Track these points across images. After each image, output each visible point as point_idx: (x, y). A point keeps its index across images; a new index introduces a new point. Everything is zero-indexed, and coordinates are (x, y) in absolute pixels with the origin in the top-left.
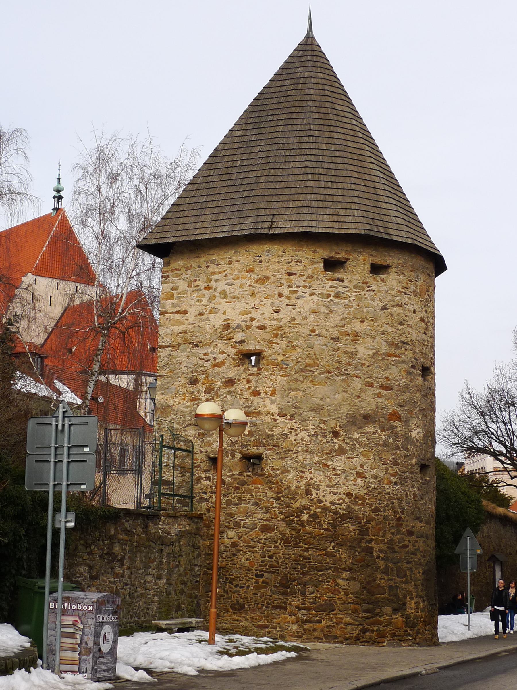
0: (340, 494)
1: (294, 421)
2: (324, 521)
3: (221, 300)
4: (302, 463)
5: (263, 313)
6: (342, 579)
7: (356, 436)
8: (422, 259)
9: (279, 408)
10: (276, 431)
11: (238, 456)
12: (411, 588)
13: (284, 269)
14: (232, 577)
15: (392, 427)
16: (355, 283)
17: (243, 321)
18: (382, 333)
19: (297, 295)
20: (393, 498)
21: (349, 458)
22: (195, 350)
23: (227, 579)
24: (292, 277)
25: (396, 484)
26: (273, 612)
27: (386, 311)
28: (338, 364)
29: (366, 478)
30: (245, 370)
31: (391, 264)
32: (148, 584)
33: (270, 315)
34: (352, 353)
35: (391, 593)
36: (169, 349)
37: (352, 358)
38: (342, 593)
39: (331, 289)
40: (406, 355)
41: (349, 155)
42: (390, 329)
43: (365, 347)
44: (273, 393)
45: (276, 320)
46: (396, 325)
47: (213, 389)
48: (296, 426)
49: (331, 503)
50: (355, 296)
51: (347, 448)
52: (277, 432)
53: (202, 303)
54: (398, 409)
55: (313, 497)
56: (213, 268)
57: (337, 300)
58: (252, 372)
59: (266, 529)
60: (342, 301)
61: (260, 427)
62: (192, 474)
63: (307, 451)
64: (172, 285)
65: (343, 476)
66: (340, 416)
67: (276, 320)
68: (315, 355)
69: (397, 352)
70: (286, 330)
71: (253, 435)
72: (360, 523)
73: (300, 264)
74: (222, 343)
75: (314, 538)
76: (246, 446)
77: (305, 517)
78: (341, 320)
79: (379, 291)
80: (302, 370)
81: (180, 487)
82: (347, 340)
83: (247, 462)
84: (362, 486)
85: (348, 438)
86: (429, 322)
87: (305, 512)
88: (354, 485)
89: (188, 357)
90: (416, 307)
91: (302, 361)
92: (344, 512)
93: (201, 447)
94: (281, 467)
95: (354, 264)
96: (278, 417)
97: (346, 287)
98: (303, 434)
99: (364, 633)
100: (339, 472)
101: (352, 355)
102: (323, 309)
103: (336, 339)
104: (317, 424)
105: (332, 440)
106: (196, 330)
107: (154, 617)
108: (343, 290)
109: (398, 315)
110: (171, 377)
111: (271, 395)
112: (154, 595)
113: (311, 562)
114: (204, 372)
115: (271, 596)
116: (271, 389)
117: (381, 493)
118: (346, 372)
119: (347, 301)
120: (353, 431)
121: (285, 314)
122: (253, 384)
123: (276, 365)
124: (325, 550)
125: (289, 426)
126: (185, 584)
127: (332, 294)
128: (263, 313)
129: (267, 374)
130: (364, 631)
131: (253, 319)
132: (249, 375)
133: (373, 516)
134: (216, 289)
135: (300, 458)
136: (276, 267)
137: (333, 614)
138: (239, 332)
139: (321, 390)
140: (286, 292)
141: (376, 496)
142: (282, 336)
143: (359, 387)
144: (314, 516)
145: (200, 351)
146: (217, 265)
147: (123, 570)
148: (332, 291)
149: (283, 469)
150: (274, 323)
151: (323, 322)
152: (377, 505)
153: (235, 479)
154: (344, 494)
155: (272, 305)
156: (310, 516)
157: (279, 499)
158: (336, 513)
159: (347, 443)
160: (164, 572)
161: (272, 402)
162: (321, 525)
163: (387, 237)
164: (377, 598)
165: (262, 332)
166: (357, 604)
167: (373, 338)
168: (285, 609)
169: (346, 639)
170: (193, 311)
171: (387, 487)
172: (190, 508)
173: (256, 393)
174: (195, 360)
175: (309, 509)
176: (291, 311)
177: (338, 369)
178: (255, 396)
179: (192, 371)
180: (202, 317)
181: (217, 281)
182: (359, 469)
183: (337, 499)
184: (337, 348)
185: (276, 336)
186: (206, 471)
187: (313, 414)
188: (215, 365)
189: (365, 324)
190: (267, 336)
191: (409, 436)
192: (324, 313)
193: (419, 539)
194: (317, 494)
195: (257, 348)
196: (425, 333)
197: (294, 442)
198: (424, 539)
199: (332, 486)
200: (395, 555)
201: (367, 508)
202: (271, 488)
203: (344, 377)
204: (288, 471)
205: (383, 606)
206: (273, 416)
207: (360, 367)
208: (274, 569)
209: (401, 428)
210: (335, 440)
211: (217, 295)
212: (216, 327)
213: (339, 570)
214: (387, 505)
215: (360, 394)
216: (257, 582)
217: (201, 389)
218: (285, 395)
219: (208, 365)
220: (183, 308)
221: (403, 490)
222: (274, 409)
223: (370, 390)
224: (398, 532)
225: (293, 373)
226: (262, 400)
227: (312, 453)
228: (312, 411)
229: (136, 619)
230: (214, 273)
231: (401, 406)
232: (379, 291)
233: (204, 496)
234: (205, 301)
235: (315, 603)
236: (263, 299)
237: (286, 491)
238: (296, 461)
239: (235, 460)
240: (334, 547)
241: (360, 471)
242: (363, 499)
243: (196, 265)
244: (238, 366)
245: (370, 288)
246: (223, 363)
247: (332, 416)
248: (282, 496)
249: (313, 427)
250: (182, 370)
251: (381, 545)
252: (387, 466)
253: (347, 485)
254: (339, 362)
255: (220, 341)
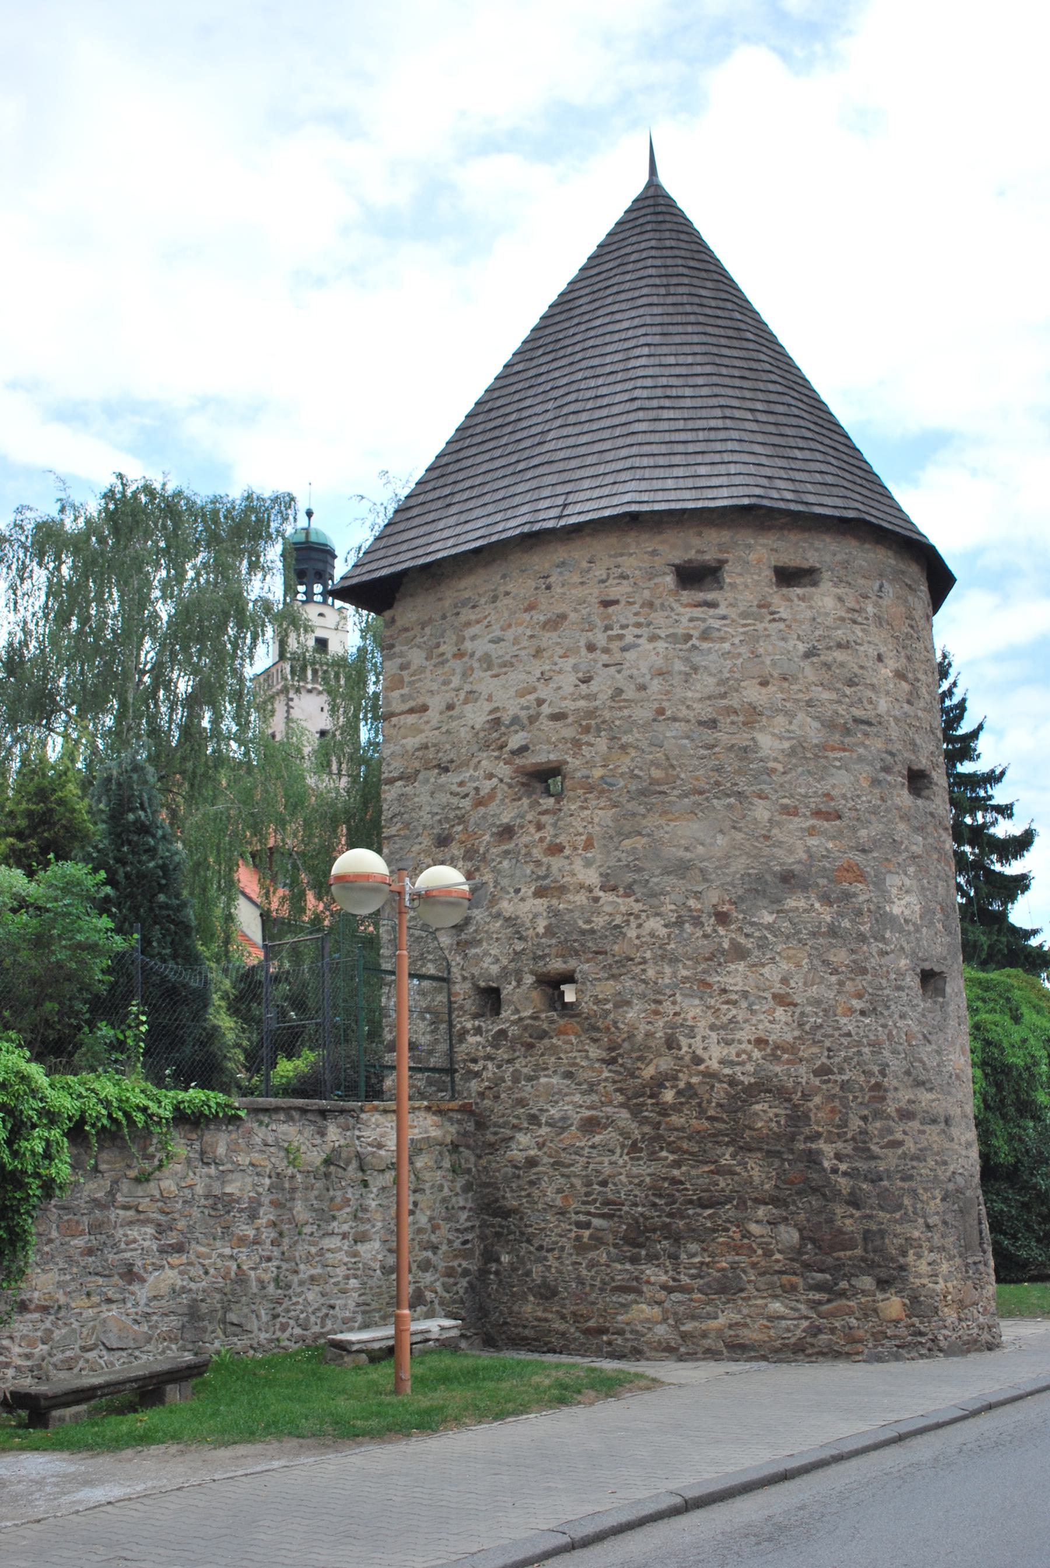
0: (740, 1042)
1: (632, 898)
2: (709, 1102)
3: (482, 674)
4: (656, 983)
5: (560, 688)
6: (757, 1222)
7: (768, 918)
8: (890, 553)
9: (601, 875)
10: (599, 922)
11: (529, 980)
12: (916, 1234)
13: (594, 593)
14: (530, 1230)
15: (847, 896)
16: (742, 607)
17: (522, 708)
18: (809, 703)
19: (623, 644)
20: (859, 1044)
21: (754, 966)
22: (443, 779)
23: (522, 1234)
24: (610, 609)
25: (863, 1013)
26: (614, 1299)
27: (815, 659)
28: (716, 774)
29: (796, 1005)
30: (531, 806)
31: (818, 565)
32: (329, 1255)
33: (572, 689)
34: (745, 749)
35: (870, 1247)
36: (400, 783)
37: (747, 758)
38: (760, 1252)
39: (692, 625)
40: (866, 747)
41: (724, 371)
42: (826, 695)
43: (773, 735)
44: (588, 845)
45: (587, 697)
46: (839, 685)
47: (477, 851)
48: (637, 907)
49: (722, 1062)
50: (744, 633)
51: (750, 946)
52: (601, 924)
53: (452, 686)
54: (859, 858)
55: (682, 1052)
56: (467, 614)
57: (705, 645)
58: (545, 807)
59: (591, 1125)
60: (717, 646)
61: (566, 917)
62: (451, 1025)
63: (663, 957)
64: (399, 661)
65: (744, 1004)
66: (729, 880)
67: (587, 697)
68: (668, 759)
69: (847, 740)
70: (607, 714)
71: (554, 935)
72: (789, 1100)
73: (625, 582)
74: (489, 757)
75: (690, 1138)
76: (542, 957)
77: (669, 1096)
78: (718, 685)
79: (795, 620)
80: (643, 793)
81: (431, 1052)
82: (733, 723)
83: (550, 991)
84: (787, 1024)
85: (753, 924)
86: (918, 680)
87: (667, 1084)
88: (770, 1022)
89: (433, 793)
90: (883, 649)
91: (641, 774)
92: (753, 1080)
93: (462, 969)
94: (612, 995)
95: (739, 570)
96: (601, 894)
97: (724, 618)
98: (654, 924)
99: (815, 1336)
100: (734, 997)
101: (745, 752)
102: (679, 666)
103: (712, 724)
104: (680, 899)
105: (715, 931)
106: (444, 738)
107: (347, 1324)
108: (717, 623)
109: (842, 665)
110: (406, 838)
111: (585, 849)
112: (347, 1278)
113: (687, 1189)
114: (461, 819)
115: (608, 1266)
116: (584, 837)
117: (832, 1036)
118: (735, 788)
119: (727, 646)
120: (759, 908)
121: (602, 685)
122: (548, 833)
123: (590, 789)
124: (716, 1161)
125: (623, 909)
126: (435, 1248)
127: (696, 633)
128: (560, 688)
129: (573, 807)
130: (815, 1331)
131: (540, 702)
132: (540, 813)
133: (817, 1083)
134: (472, 655)
135: (651, 973)
136: (578, 592)
137: (743, 1299)
138: (516, 732)
139: (688, 829)
140: (600, 639)
141: (820, 1042)
142: (599, 730)
143: (766, 818)
144: (688, 1092)
145: (451, 779)
146: (474, 607)
147: (258, 1229)
148: (694, 628)
149: (618, 998)
150: (582, 703)
151: (679, 693)
152: (825, 1060)
153: (526, 1028)
154: (749, 1042)
155: (575, 668)
156: (679, 1093)
157: (613, 1061)
158: (732, 1082)
159: (747, 935)
160: (373, 1226)
161: (588, 863)
162: (702, 1111)
163: (801, 508)
164: (838, 1259)
165: (559, 724)
166: (795, 1274)
167: (791, 715)
168: (639, 1292)
169: (777, 1351)
170: (436, 704)
171: (844, 1020)
172: (450, 1093)
173: (556, 849)
174: (443, 798)
175: (676, 1078)
176: (613, 678)
177: (718, 784)
178: (553, 854)
179: (440, 821)
180: (451, 713)
181: (473, 638)
182: (778, 988)
183: (734, 1052)
184: (713, 742)
185: (587, 730)
186: (475, 1016)
187: (672, 880)
188: (480, 803)
189: (771, 689)
190: (569, 733)
191: (885, 912)
192: (680, 673)
193: (927, 1128)
194: (690, 1046)
195: (552, 757)
196: (909, 702)
197: (637, 942)
198: (942, 1125)
199: (723, 1027)
200: (873, 1164)
201: (802, 1070)
202: (595, 1041)
203: (732, 800)
204: (628, 1003)
205: (853, 1275)
206: (591, 891)
207: (765, 777)
208: (611, 1209)
209: (866, 897)
210: (721, 931)
211: (476, 665)
212: (477, 727)
213: (749, 1203)
214: (846, 1059)
215: (769, 831)
216: (578, 1238)
217: (456, 852)
218: (611, 846)
219: (466, 803)
220: (420, 701)
221: (882, 1026)
222: (591, 877)
223: (790, 822)
224: (878, 1115)
225: (623, 800)
226: (567, 862)
227: (674, 960)
228: (669, 873)
229: (298, 1331)
230: (468, 624)
231: (864, 851)
232: (795, 620)
233: (472, 1066)
234: (456, 681)
235: (702, 1277)
236: (556, 659)
237: (626, 1045)
238: (644, 981)
239: (524, 987)
240: (733, 1156)
241: (782, 992)
242: (792, 1049)
243: (437, 616)
244: (519, 799)
245: (776, 616)
246: (491, 796)
247: (712, 881)
248: (619, 1055)
249: (673, 907)
250: (423, 821)
251: (840, 1145)
252: (842, 977)
253: (754, 1022)
254: (719, 769)
255: (485, 754)
